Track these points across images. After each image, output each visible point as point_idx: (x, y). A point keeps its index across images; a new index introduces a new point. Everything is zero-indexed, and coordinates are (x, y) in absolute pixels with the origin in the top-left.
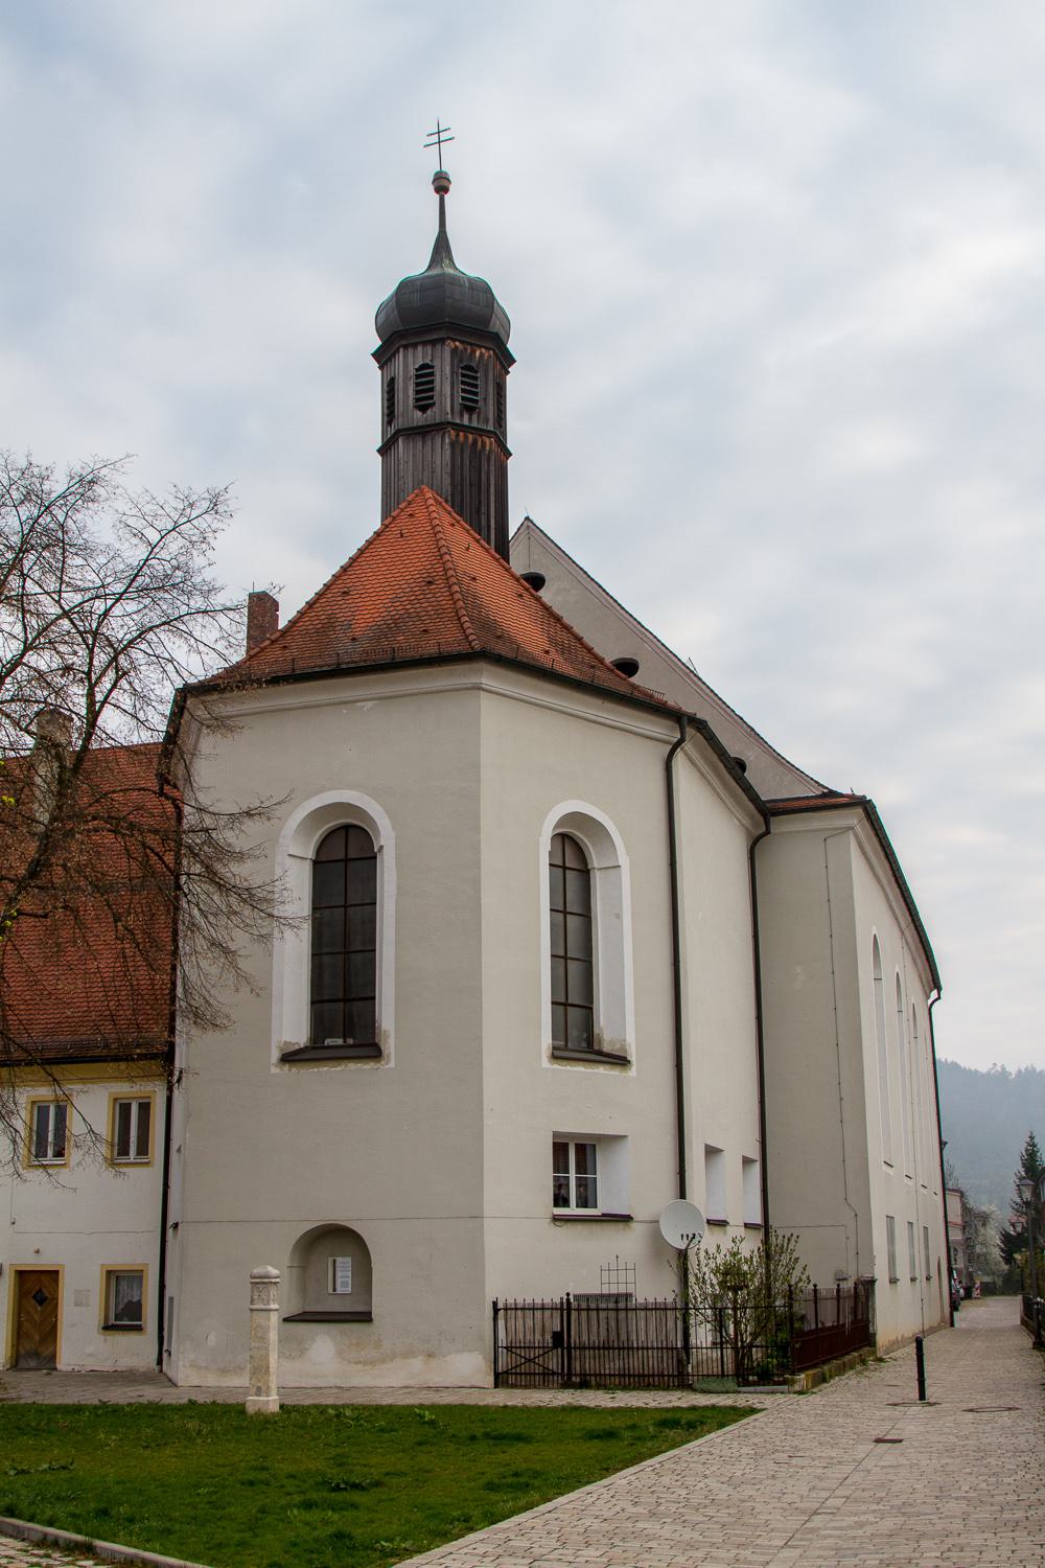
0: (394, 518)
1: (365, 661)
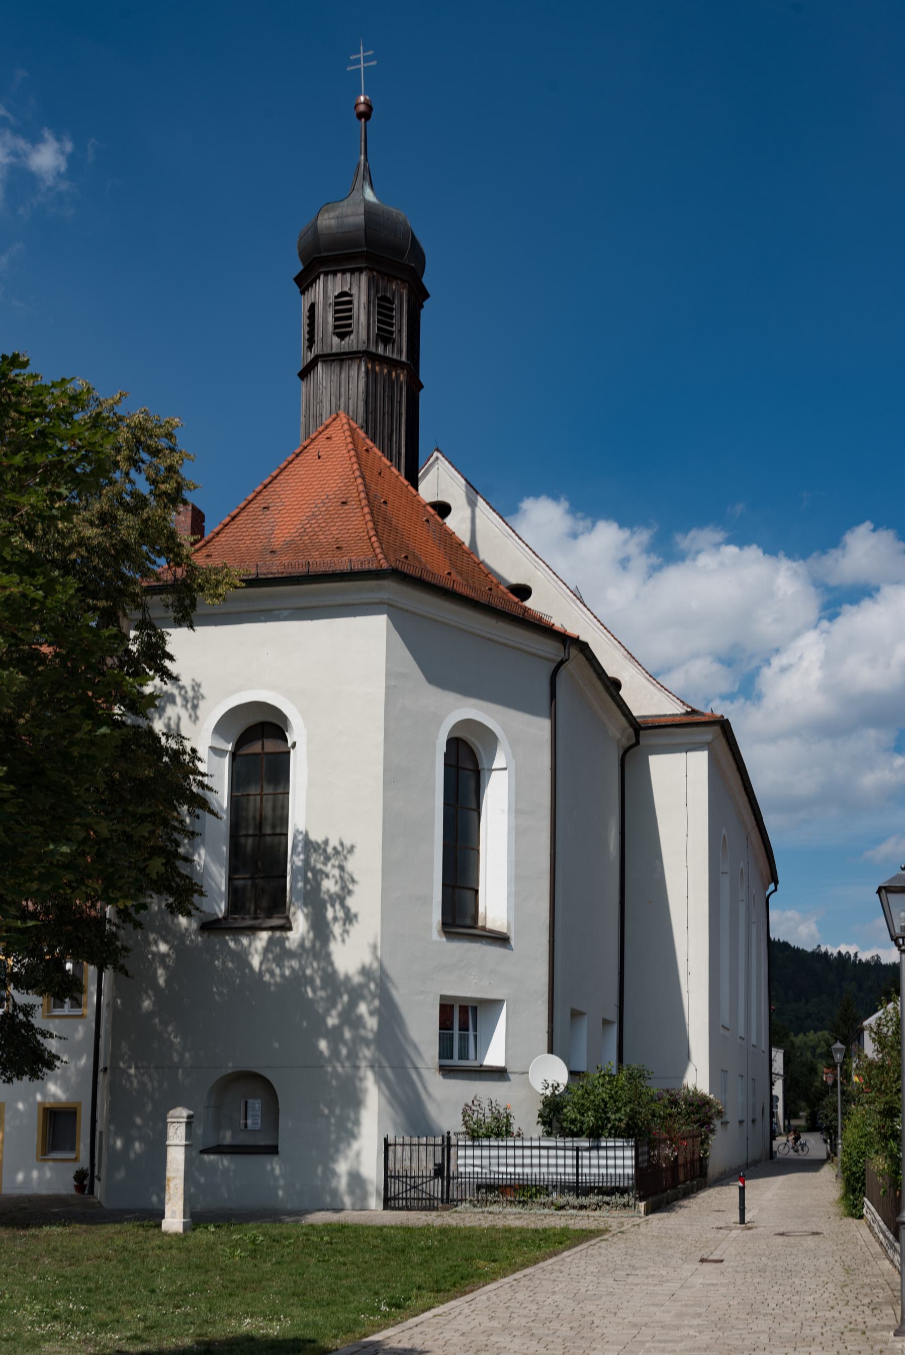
0: (313, 440)
1: (282, 573)
